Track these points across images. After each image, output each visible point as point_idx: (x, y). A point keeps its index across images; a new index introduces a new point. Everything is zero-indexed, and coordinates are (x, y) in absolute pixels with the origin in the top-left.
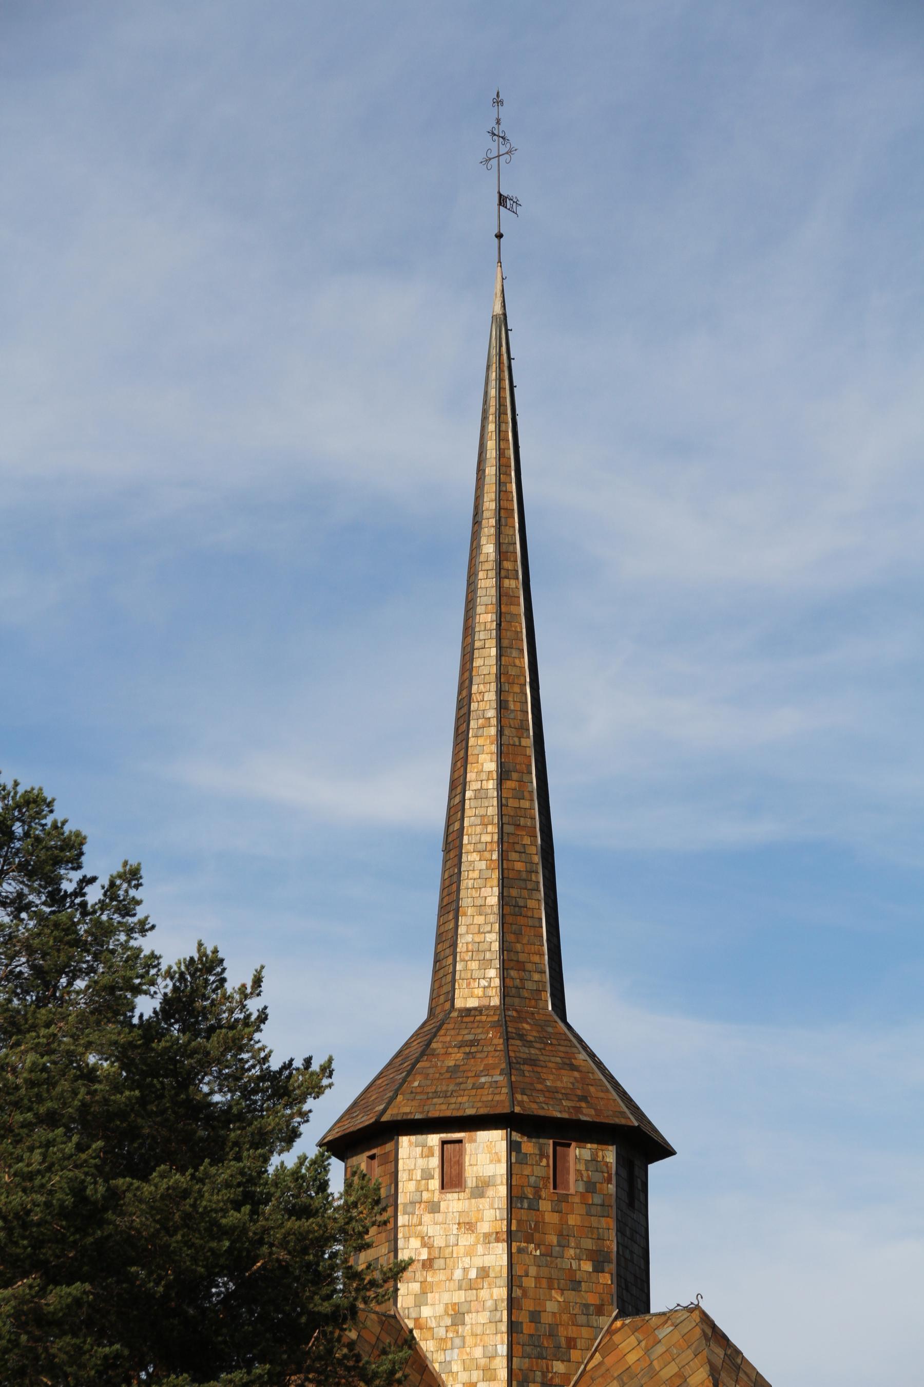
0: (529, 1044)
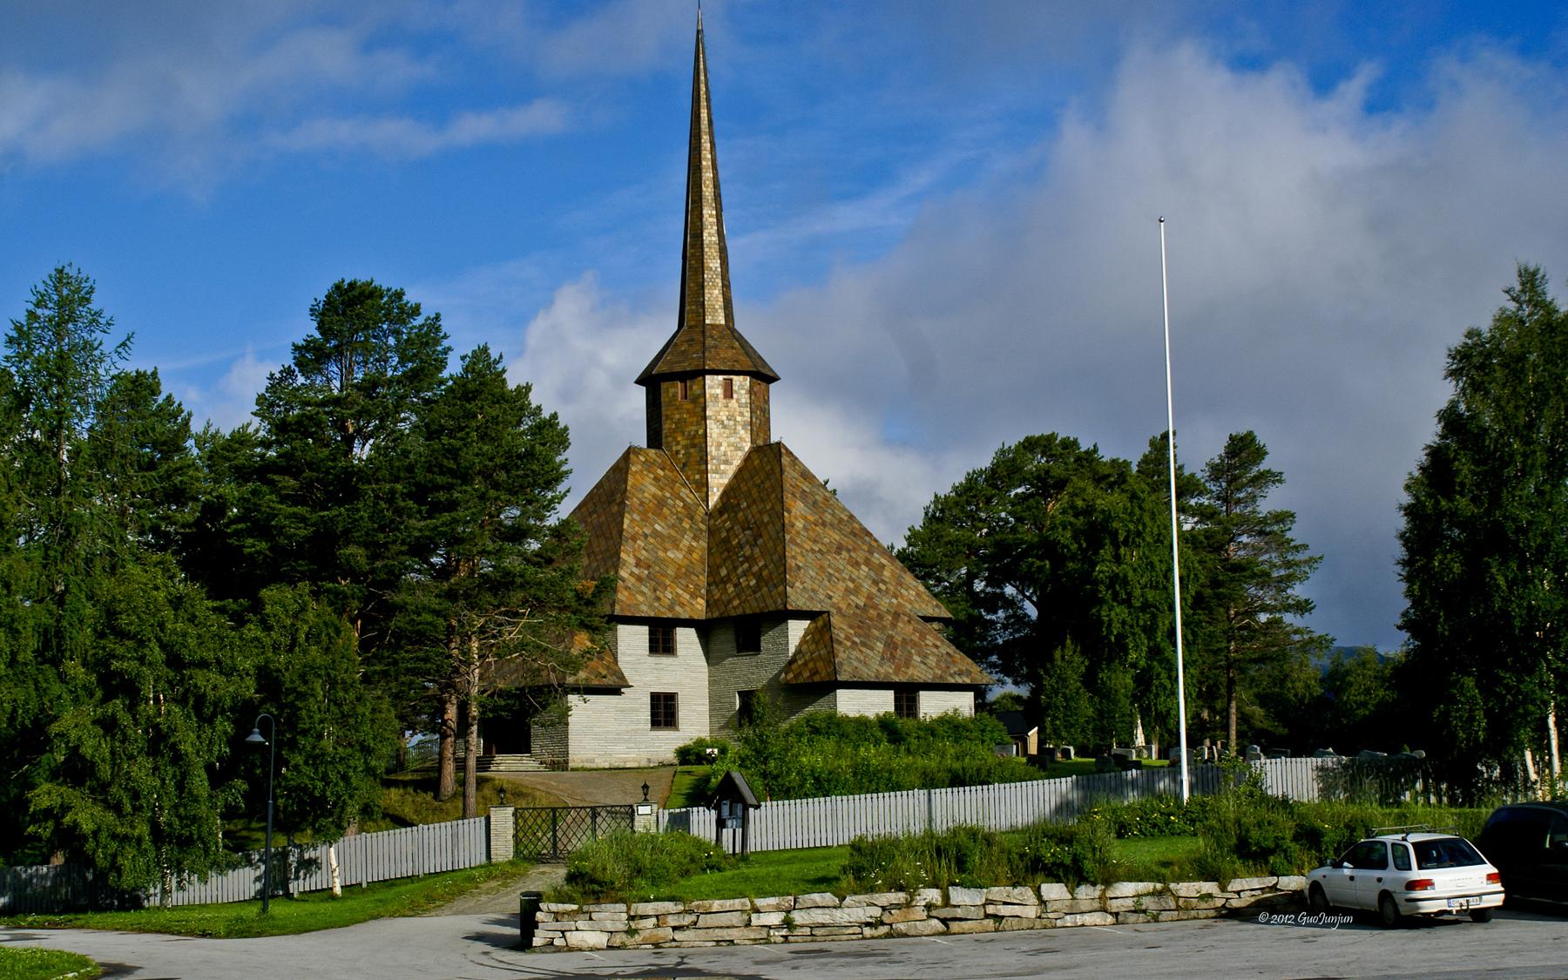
0: (716, 340)
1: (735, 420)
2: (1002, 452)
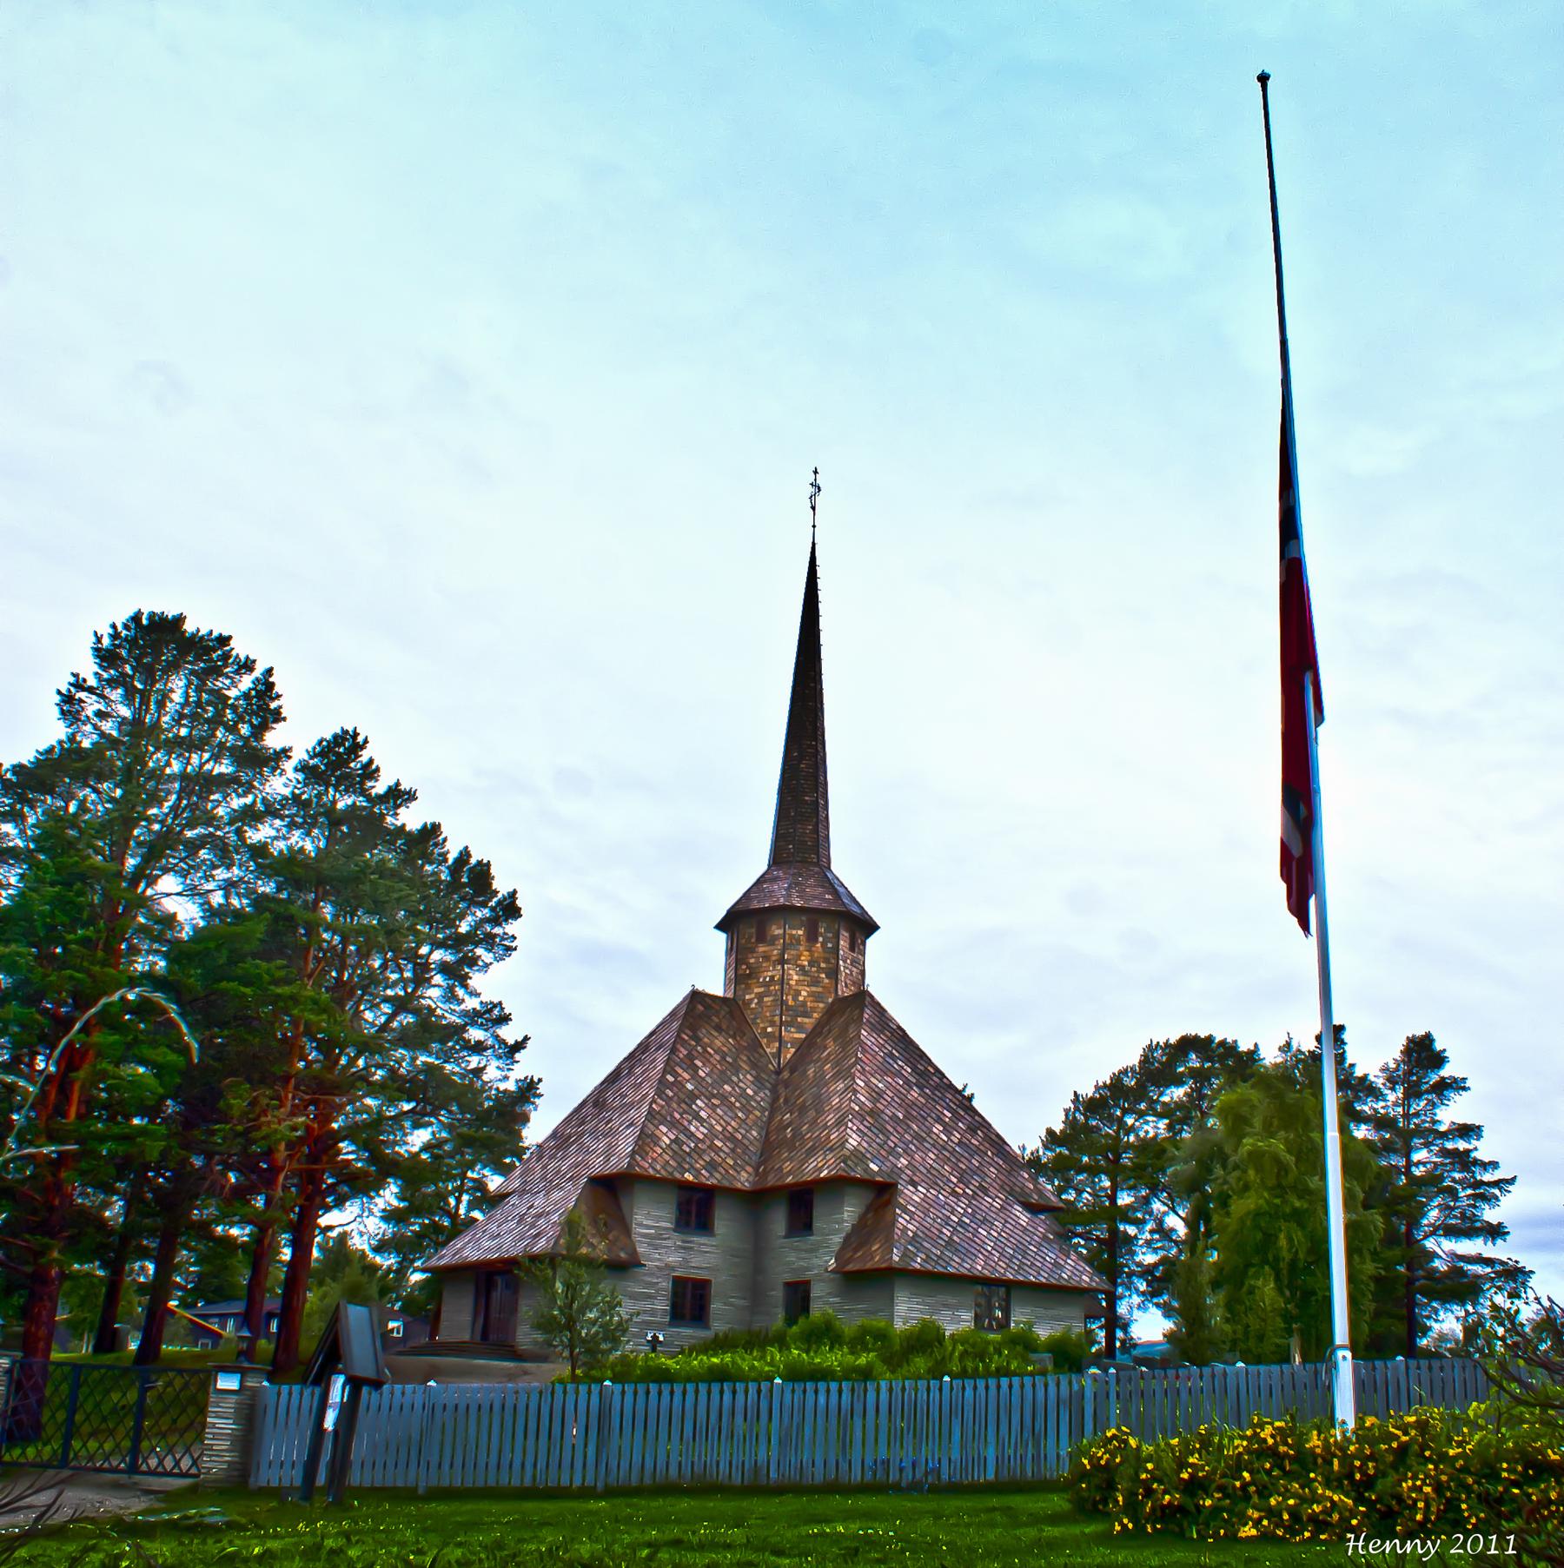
1: (819, 966)
2: (1151, 1048)
